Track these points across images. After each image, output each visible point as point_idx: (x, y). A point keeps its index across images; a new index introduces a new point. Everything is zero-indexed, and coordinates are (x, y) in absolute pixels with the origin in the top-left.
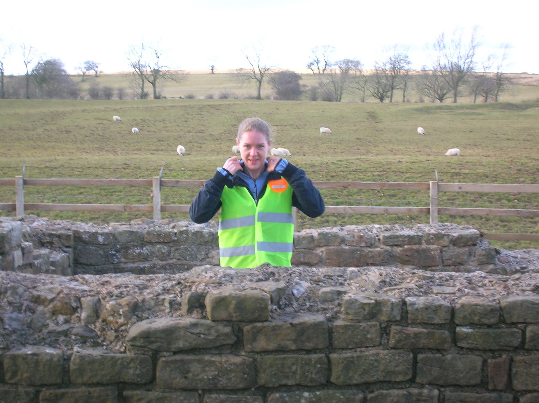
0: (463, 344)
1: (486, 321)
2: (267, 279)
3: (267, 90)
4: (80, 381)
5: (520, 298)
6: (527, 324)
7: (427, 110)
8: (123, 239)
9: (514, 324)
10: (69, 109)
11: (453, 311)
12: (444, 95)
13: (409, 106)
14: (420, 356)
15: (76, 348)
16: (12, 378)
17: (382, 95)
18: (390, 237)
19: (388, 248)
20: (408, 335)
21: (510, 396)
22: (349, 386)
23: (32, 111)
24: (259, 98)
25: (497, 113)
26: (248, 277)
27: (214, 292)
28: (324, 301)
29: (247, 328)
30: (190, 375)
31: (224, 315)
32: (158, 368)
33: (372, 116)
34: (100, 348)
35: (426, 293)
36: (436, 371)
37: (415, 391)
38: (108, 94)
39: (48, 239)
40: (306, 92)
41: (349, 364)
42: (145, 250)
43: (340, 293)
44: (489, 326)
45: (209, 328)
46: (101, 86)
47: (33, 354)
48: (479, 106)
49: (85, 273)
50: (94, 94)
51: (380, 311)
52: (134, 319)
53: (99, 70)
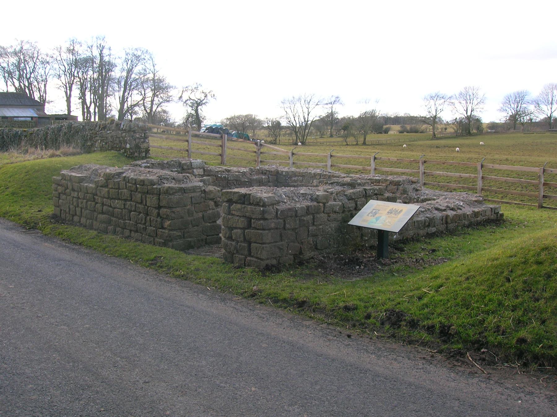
39: (265, 172)
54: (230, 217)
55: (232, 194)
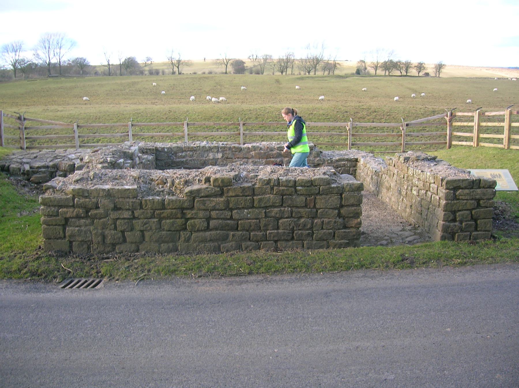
0: (299, 193)
1: (306, 185)
2: (231, 171)
3: (230, 69)
4: (168, 208)
5: (318, 177)
6: (320, 186)
7: (302, 79)
8: (175, 150)
9: (316, 186)
10: (140, 80)
11: (295, 182)
12: (310, 71)
13: (294, 77)
14: (284, 197)
15: (166, 197)
16: (145, 207)
17: (282, 71)
18: (279, 147)
19: (279, 151)
20: (280, 190)
21: (315, 210)
22: (260, 208)
23: (123, 81)
24: (226, 73)
25: (333, 80)
26: (225, 171)
27: (213, 177)
28: (251, 179)
29: (225, 189)
30: (206, 205)
31: (217, 184)
32: (195, 203)
33: (278, 81)
34: (175, 196)
35: (286, 175)
36: (290, 202)
37: (282, 209)
38: (157, 73)
39: (145, 151)
40: (247, 69)
41: (260, 200)
42: (184, 154)
43: (257, 176)
44: (308, 187)
45: (212, 189)
46: (154, 68)
47: (152, 199)
48: (326, 77)
49: (167, 169)
50: (151, 73)
51: (270, 182)
52: (186, 186)
53: (152, 61)
54: (455, 202)
55: (461, 181)
